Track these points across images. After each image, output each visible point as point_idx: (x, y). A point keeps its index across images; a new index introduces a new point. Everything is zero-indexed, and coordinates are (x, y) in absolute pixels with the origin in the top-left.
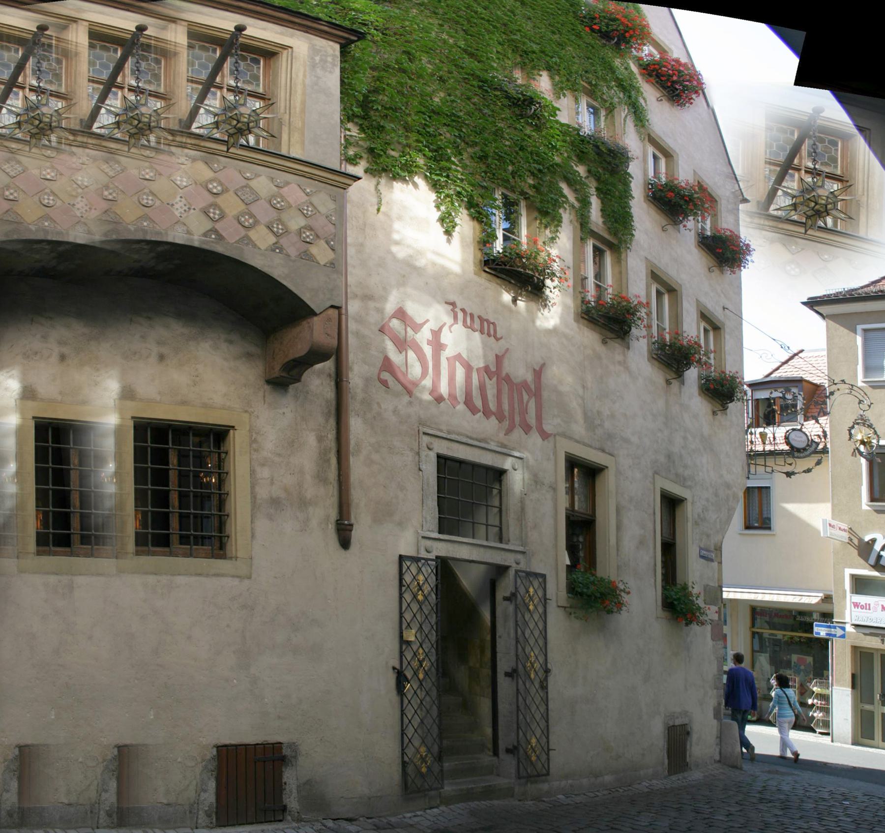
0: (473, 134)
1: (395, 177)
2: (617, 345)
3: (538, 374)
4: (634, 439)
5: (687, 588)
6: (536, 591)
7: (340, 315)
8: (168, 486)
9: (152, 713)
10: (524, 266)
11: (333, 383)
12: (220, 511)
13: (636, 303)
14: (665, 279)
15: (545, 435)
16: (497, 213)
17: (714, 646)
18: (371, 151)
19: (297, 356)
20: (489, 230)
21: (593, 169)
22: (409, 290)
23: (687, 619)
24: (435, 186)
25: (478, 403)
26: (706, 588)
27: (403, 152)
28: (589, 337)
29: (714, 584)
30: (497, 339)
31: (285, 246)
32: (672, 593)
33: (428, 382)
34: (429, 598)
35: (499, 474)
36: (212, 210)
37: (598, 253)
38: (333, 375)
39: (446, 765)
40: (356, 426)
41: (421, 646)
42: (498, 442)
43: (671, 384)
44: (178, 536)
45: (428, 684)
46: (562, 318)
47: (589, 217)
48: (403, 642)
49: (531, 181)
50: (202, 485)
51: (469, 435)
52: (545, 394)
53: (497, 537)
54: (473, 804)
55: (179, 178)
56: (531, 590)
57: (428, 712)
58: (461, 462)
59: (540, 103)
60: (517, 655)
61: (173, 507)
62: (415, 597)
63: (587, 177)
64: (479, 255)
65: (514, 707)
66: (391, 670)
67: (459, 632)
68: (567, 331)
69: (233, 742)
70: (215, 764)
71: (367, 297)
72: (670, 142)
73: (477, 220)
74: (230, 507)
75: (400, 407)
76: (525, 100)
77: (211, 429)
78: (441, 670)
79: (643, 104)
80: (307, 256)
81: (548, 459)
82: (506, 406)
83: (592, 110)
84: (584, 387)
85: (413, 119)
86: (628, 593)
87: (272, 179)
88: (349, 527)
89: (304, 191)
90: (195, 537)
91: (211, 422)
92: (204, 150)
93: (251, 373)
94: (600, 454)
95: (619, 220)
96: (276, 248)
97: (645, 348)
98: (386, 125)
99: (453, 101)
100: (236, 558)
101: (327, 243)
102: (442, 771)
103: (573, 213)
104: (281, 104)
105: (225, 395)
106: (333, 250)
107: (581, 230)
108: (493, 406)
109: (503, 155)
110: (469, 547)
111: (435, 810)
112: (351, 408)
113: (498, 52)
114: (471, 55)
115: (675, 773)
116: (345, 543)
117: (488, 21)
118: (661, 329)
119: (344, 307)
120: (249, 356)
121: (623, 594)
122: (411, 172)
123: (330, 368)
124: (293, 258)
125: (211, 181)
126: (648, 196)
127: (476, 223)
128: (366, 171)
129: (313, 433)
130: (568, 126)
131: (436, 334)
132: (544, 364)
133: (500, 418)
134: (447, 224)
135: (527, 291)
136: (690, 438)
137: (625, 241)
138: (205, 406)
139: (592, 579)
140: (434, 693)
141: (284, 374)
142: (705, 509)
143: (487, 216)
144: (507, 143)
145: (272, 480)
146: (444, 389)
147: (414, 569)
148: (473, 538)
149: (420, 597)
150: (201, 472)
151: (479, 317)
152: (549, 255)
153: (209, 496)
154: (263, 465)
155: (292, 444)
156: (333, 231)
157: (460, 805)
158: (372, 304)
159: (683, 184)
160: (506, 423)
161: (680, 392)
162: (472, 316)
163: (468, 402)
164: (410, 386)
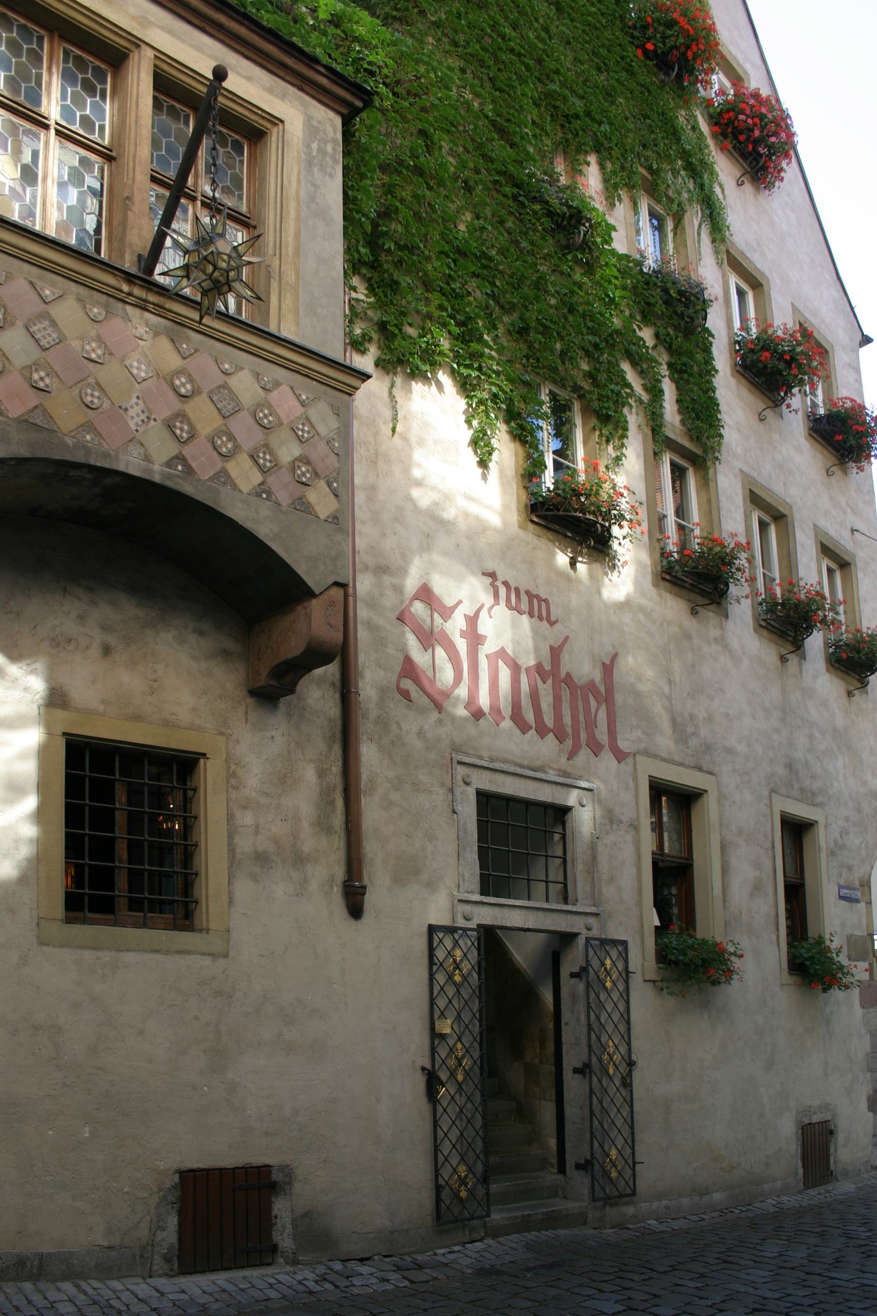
0: (510, 289)
1: (415, 374)
2: (711, 614)
3: (608, 669)
4: (742, 748)
5: (824, 942)
6: (614, 963)
7: (346, 596)
8: (114, 804)
9: (87, 1129)
10: (583, 509)
11: (337, 696)
12: (185, 812)
13: (732, 545)
14: (768, 500)
15: (620, 756)
16: (544, 426)
17: (864, 1016)
18: (382, 327)
19: (290, 656)
20: (535, 456)
21: (662, 331)
22: (436, 557)
23: (824, 984)
24: (465, 387)
25: (530, 717)
26: (850, 939)
27: (423, 328)
28: (672, 608)
29: (860, 932)
30: (552, 624)
31: (274, 489)
32: (803, 951)
33: (462, 692)
34: (470, 979)
35: (561, 813)
36: (178, 424)
37: (678, 473)
38: (338, 684)
39: (494, 1187)
40: (369, 755)
41: (459, 1039)
42: (559, 770)
43: (787, 661)
44: (127, 899)
45: (469, 1088)
46: (636, 583)
47: (662, 416)
48: (435, 1036)
49: (585, 367)
50: (161, 833)
51: (518, 761)
52: (619, 698)
53: (561, 897)
54: (532, 1235)
55: (135, 364)
56: (608, 962)
57: (469, 1121)
58: (509, 800)
59: (589, 220)
60: (590, 1046)
61: (120, 861)
62: (450, 977)
63: (655, 347)
64: (524, 497)
65: (587, 1111)
66: (420, 1071)
67: (511, 1020)
68: (644, 602)
69: (203, 1166)
70: (177, 1194)
71: (382, 570)
72: (760, 261)
73: (520, 440)
74: (199, 861)
75: (426, 727)
76: (571, 217)
77: (174, 756)
78: (486, 1069)
79: (721, 197)
80: (302, 506)
81: (627, 788)
82: (567, 720)
83: (655, 223)
84: (670, 682)
85: (435, 267)
86: (741, 956)
87: (257, 376)
88: (360, 890)
89: (298, 397)
90: (151, 902)
91: (174, 747)
92: (170, 315)
93: (228, 680)
94: (698, 774)
95: (702, 413)
96: (263, 491)
97: (749, 612)
98: (401, 280)
99: (482, 229)
100: (208, 930)
101: (329, 485)
102: (488, 1194)
103: (642, 413)
104: (270, 238)
105: (194, 709)
106: (336, 496)
107: (654, 439)
108: (549, 720)
109: (548, 324)
110: (523, 912)
111: (477, 1244)
112: (362, 730)
113: (534, 122)
114: (503, 133)
115: (815, 1186)
116: (355, 910)
117: (519, 55)
118: (768, 580)
119: (351, 585)
120: (226, 655)
121: (733, 958)
122: (433, 364)
123: (333, 675)
124: (285, 508)
125: (179, 373)
126: (736, 364)
127: (518, 443)
128: (377, 365)
129: (312, 765)
130: (627, 257)
131: (472, 621)
132: (616, 655)
133: (560, 738)
134: (481, 445)
135: (588, 547)
136: (817, 735)
137: (712, 448)
138: (166, 723)
139: (690, 942)
140: (478, 1098)
141: (272, 682)
142: (844, 832)
143: (532, 433)
144: (553, 302)
145: (257, 827)
146: (484, 700)
147: (448, 943)
148: (529, 899)
149: (457, 978)
150: (161, 814)
151: (527, 592)
152: (614, 487)
153: (170, 848)
154: (245, 808)
155: (285, 780)
156: (337, 465)
157: (514, 1237)
158: (387, 580)
159: (780, 333)
160: (569, 743)
161: (801, 672)
162: (517, 590)
163: (517, 716)
164: (439, 698)
